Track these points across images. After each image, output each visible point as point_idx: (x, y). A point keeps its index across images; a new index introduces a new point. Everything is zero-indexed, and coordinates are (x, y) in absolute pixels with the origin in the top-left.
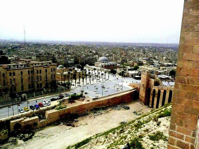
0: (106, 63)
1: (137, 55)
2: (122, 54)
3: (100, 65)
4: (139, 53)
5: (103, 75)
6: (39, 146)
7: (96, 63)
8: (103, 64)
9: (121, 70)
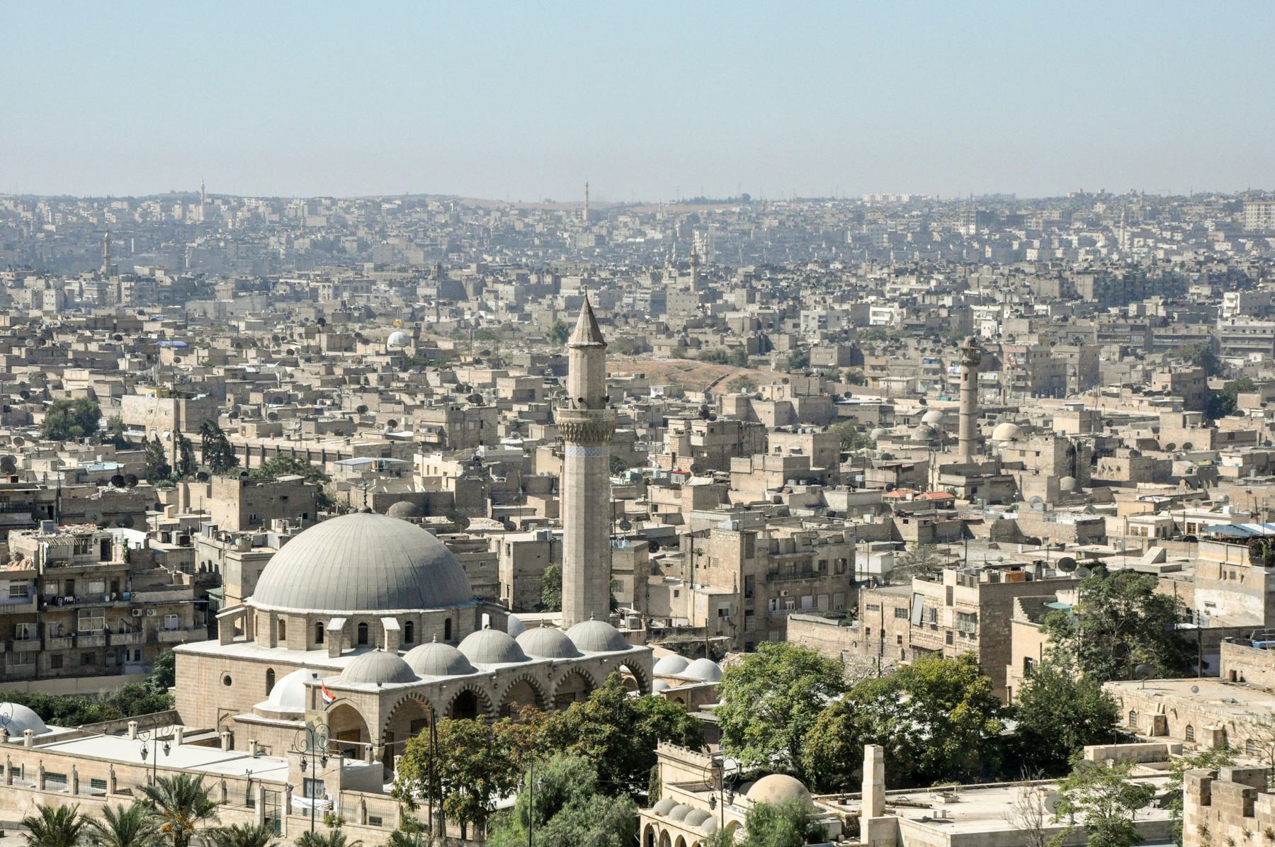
0: (409, 637)
1: (1042, 455)
2: (741, 438)
3: (290, 692)
4: (1091, 420)
5: (1172, 776)
6: (890, 799)
7: (198, 672)
8: (357, 675)
9: (738, 783)
